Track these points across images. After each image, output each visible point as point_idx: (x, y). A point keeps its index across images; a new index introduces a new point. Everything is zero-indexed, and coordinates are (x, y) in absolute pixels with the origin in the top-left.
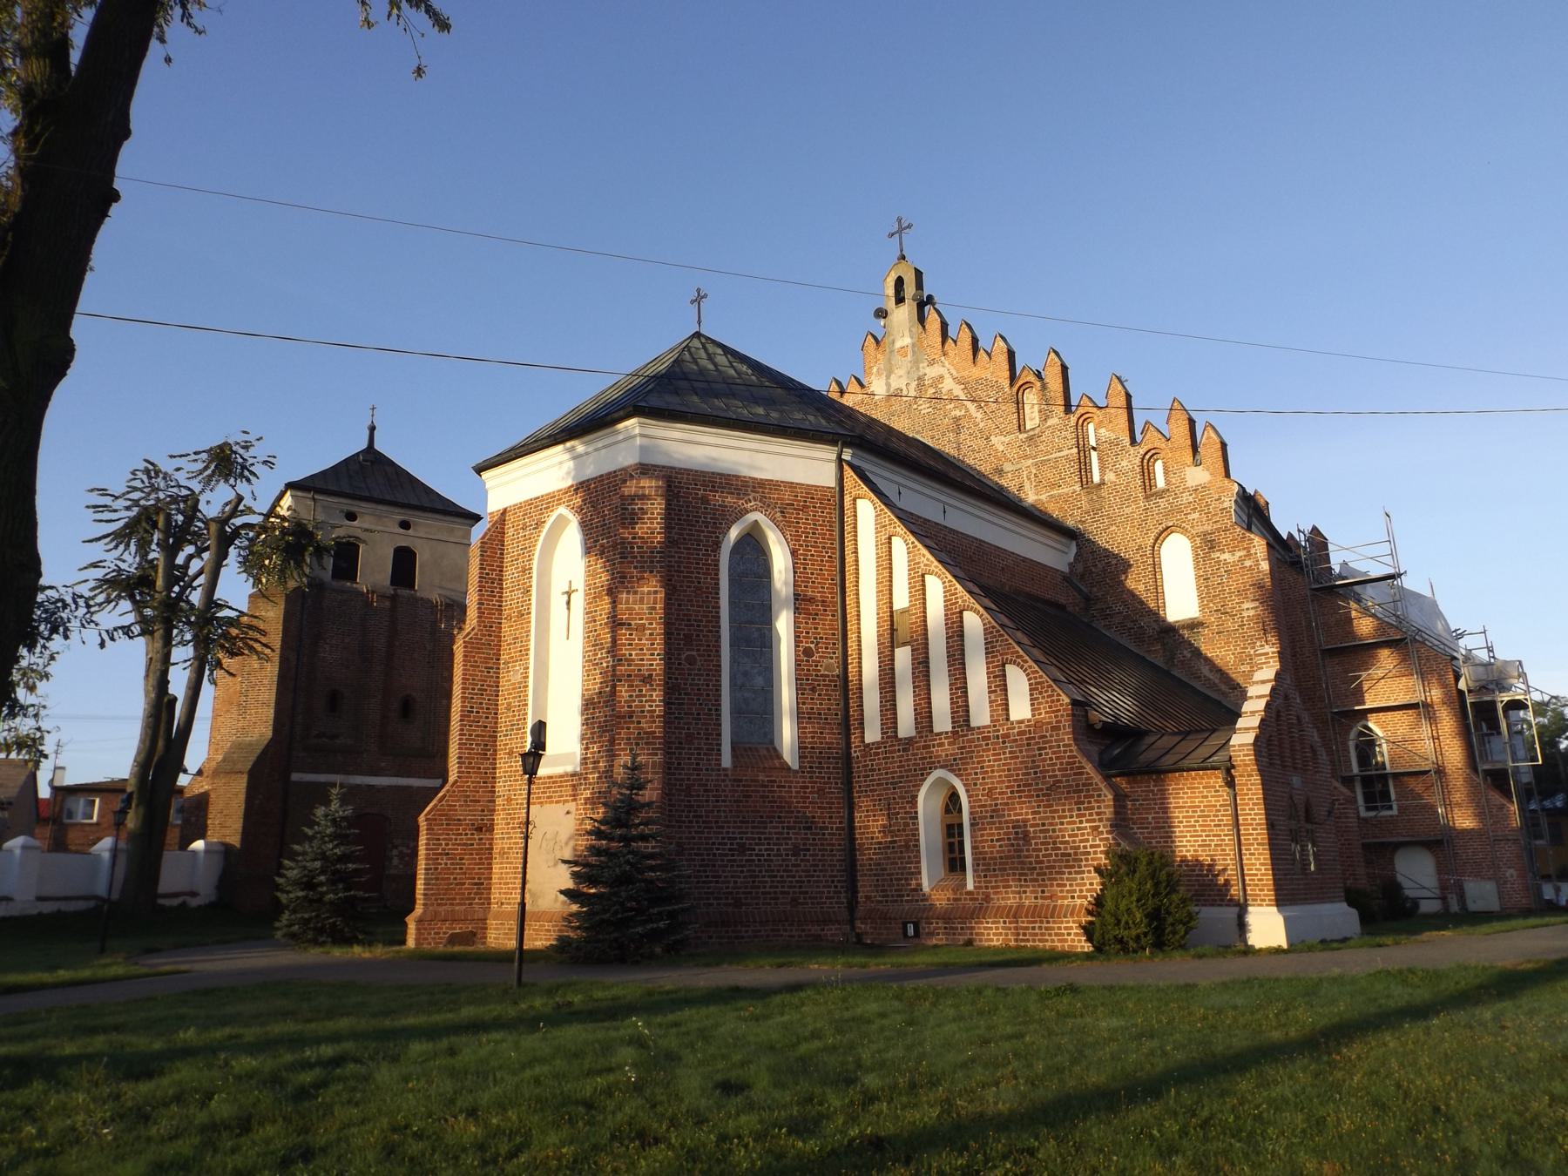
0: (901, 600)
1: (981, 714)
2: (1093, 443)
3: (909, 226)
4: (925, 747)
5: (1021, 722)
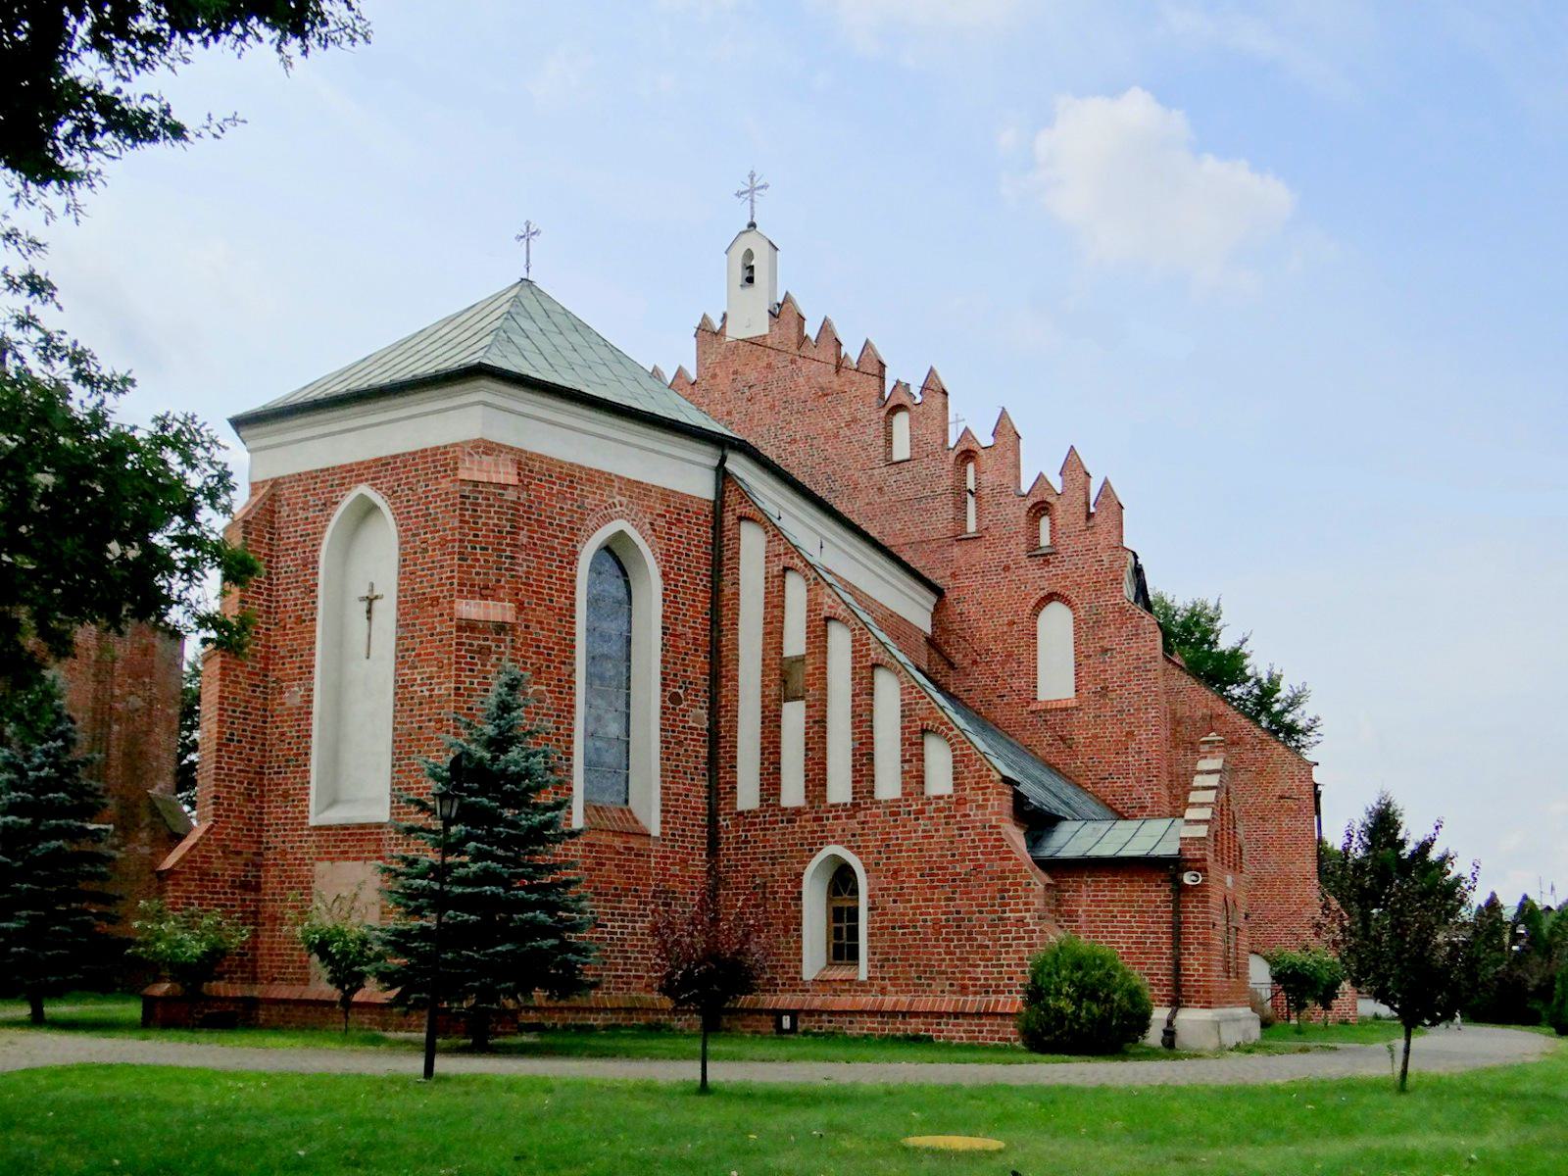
0: (795, 643)
1: (888, 785)
2: (971, 485)
3: (739, 194)
4: (815, 819)
5: (940, 797)
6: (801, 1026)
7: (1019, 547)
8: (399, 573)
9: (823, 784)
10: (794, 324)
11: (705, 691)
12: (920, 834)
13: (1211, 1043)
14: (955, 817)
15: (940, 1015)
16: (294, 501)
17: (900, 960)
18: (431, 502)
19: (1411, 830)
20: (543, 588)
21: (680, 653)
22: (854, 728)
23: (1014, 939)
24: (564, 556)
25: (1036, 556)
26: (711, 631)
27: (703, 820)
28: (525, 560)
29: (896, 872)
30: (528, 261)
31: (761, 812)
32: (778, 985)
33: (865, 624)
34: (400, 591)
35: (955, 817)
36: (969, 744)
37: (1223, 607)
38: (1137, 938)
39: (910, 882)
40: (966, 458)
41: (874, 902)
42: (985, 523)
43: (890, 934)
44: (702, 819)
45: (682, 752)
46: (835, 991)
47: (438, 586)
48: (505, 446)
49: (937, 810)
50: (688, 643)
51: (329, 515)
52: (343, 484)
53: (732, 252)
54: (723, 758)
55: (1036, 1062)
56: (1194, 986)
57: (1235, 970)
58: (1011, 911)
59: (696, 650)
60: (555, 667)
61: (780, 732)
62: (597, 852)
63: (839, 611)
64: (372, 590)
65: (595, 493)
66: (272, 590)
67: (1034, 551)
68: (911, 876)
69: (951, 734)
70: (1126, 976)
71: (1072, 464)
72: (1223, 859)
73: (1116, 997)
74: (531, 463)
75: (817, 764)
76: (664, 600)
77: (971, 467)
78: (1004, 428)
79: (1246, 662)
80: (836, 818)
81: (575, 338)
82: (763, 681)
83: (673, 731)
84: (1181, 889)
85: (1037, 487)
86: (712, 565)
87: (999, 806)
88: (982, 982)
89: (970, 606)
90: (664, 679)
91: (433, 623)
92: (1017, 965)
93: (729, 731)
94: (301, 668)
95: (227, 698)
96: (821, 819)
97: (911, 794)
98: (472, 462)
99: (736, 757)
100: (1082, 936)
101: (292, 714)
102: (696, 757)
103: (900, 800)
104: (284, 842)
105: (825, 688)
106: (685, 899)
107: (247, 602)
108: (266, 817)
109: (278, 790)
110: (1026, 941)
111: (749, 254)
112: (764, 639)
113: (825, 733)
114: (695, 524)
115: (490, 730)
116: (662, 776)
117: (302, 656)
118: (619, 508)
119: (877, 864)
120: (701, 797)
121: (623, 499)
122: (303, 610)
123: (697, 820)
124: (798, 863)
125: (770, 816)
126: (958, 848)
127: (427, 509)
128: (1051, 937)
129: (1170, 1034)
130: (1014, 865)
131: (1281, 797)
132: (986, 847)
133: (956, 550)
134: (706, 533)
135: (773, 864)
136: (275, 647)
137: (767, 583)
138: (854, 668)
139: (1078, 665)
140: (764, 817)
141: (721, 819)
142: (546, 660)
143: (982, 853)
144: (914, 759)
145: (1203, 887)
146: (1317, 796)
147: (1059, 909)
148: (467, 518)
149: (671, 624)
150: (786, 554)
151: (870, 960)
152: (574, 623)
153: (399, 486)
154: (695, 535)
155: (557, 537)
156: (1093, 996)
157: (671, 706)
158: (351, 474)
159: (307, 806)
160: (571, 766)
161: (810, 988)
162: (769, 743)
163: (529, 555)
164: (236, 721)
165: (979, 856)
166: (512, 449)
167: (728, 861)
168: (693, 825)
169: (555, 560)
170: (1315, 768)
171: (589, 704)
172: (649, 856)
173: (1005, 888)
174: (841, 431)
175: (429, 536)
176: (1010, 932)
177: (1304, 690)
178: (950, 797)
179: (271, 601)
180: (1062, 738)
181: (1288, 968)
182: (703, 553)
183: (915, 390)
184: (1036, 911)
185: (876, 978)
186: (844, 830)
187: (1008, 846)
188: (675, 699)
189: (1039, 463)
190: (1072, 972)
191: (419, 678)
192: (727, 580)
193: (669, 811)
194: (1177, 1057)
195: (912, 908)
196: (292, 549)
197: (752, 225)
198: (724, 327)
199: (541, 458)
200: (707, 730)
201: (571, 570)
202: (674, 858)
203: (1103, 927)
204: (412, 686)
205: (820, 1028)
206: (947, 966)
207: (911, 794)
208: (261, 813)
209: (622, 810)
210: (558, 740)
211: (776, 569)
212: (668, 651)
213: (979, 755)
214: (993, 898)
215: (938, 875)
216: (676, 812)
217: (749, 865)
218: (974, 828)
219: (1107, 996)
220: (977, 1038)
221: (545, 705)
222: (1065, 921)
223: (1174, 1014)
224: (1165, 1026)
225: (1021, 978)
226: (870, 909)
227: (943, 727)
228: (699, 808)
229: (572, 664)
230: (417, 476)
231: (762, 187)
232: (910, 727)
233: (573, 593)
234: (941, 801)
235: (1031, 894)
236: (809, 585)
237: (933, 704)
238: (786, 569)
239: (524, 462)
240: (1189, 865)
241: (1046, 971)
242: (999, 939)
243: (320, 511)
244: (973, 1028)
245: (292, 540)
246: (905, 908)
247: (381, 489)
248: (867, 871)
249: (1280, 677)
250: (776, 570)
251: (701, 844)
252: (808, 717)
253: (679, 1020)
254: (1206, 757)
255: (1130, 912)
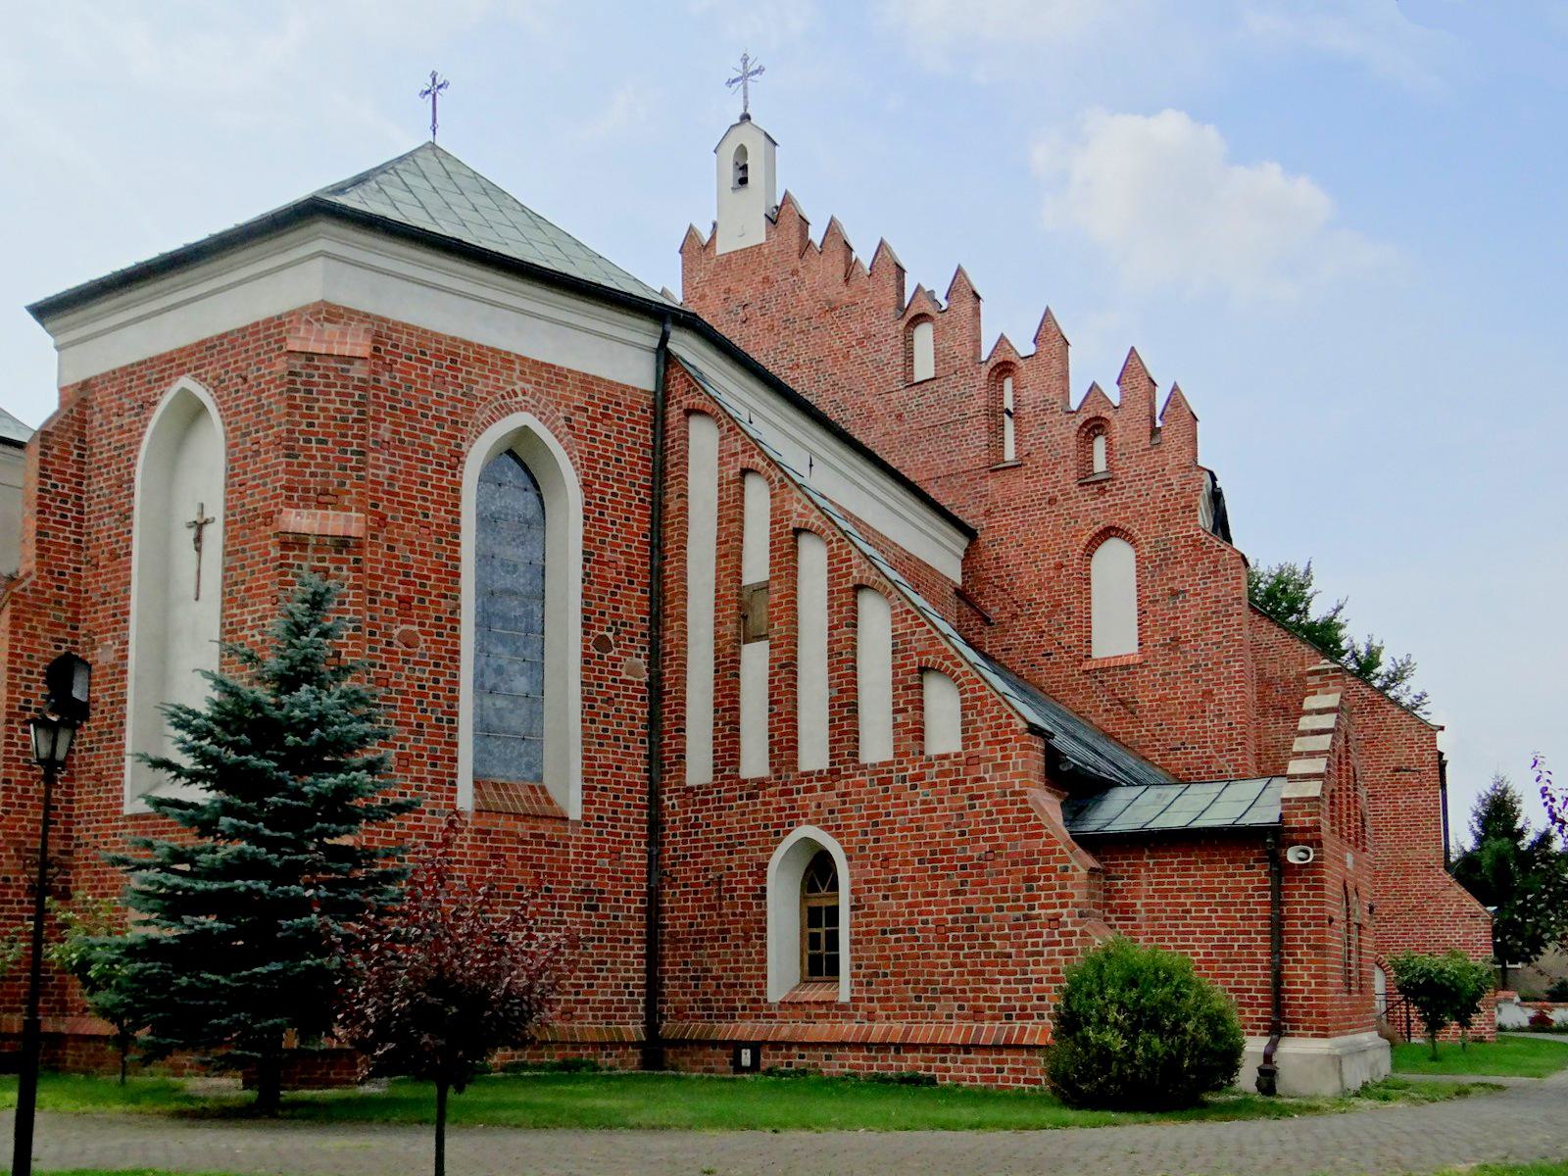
0: (756, 567)
1: (877, 744)
2: (1009, 404)
4: (783, 793)
5: (946, 757)
6: (766, 1062)
7: (1066, 477)
8: (226, 486)
9: (793, 746)
10: (795, 227)
11: (643, 635)
12: (918, 806)
13: (1329, 1087)
14: (964, 781)
15: (945, 1048)
16: (107, 405)
17: (893, 974)
18: (263, 391)
19: (1531, 818)
20: (415, 498)
21: (609, 585)
22: (831, 671)
23: (1045, 945)
24: (443, 458)
25: (1088, 484)
26: (651, 558)
27: (641, 799)
28: (390, 462)
29: (886, 859)
30: (434, 121)
31: (714, 786)
32: (736, 1009)
33: (844, 533)
34: (228, 508)
35: (964, 781)
36: (983, 683)
37: (1314, 572)
38: (1219, 940)
39: (904, 871)
40: (1000, 373)
41: (858, 900)
42: (1026, 447)
43: (879, 941)
44: (640, 798)
45: (612, 712)
46: (809, 1016)
47: (273, 497)
48: (357, 312)
49: (941, 774)
50: (619, 573)
51: (146, 419)
52: (162, 379)
53: (720, 151)
54: (668, 719)
55: (1066, 1125)
56: (1301, 1006)
57: (1355, 983)
58: (1043, 906)
59: (631, 582)
60: (431, 602)
61: (738, 683)
62: (493, 840)
63: (812, 520)
64: (202, 514)
65: (487, 377)
66: (83, 520)
67: (1086, 479)
68: (906, 863)
69: (958, 671)
70: (1203, 995)
71: (1133, 370)
72: (1341, 829)
73: (1189, 1026)
74: (394, 335)
75: (784, 721)
76: (586, 518)
77: (1008, 383)
78: (1048, 332)
79: (1341, 633)
80: (809, 790)
81: (481, 201)
82: (716, 618)
83: (600, 686)
84: (1282, 871)
85: (1089, 401)
86: (652, 475)
87: (1025, 766)
88: (1002, 1003)
89: (1006, 545)
90: (587, 619)
91: (266, 546)
92: (1050, 980)
93: (675, 685)
94: (114, 615)
95: (20, 656)
96: (790, 792)
97: (906, 754)
98: (308, 331)
99: (684, 718)
100: (1141, 938)
101: (107, 674)
102: (633, 719)
103: (891, 763)
104: (96, 836)
105: (794, 622)
106: (617, 900)
107: (47, 535)
108: (76, 805)
109: (89, 771)
110: (1063, 947)
111: (742, 151)
112: (718, 564)
113: (795, 680)
114: (628, 420)
115: (273, 663)
116: (583, 743)
117: (116, 600)
118: (521, 398)
119: (862, 849)
120: (639, 770)
121: (527, 386)
122: (117, 542)
123: (634, 799)
124: (761, 850)
125: (726, 791)
126: (970, 824)
127: (259, 400)
128: (1097, 941)
129: (1268, 1078)
130: (1045, 844)
131: (1397, 770)
132: (1006, 820)
133: (990, 482)
134: (644, 434)
135: (730, 853)
136: (87, 592)
137: (720, 491)
138: (831, 593)
139: (1142, 612)
140: (719, 792)
141: (665, 797)
142: (419, 592)
143: (1001, 829)
144: (910, 708)
145: (1315, 868)
146: (1442, 766)
147: (1111, 905)
148: (298, 402)
149: (596, 548)
150: (744, 452)
151: (853, 975)
152: (459, 545)
153: (227, 372)
154: (629, 435)
155: (434, 433)
156: (1154, 1025)
157: (597, 653)
158: (168, 365)
159: (122, 789)
160: (456, 729)
161: (777, 1012)
162: (723, 697)
163: (393, 455)
164: (33, 685)
165: (998, 834)
166: (367, 316)
167: (675, 850)
168: (628, 806)
169: (431, 463)
170: (1439, 734)
171: (481, 650)
172: (566, 846)
173: (1033, 873)
174: (852, 351)
175: (261, 434)
176: (1040, 935)
177: (1408, 663)
178: (957, 755)
179: (82, 535)
180: (1122, 702)
181: (1420, 977)
182: (639, 458)
183: (940, 297)
184: (1076, 905)
185: (862, 999)
186: (819, 806)
187: (1036, 819)
188: (602, 644)
189: (1092, 369)
190: (1123, 990)
191: (250, 618)
192: (672, 493)
193: (594, 788)
194: (1282, 1112)
195: (909, 905)
196: (106, 466)
197: (746, 117)
198: (713, 237)
199: (410, 330)
200: (647, 684)
201: (454, 475)
202: (602, 848)
203: (1171, 926)
204: (242, 629)
205: (789, 1064)
206: (955, 983)
207: (906, 754)
208: (70, 802)
209: (532, 788)
210: (436, 696)
211: (732, 472)
212: (591, 583)
213: (997, 698)
214: (1016, 890)
215: (942, 861)
216: (604, 789)
217: (701, 855)
218: (990, 796)
219: (1176, 1024)
220: (995, 1079)
221: (418, 650)
222: (1117, 919)
223: (1273, 1045)
224: (1261, 1062)
225: (1053, 1001)
226: (853, 908)
227: (947, 663)
228: (636, 784)
229: (456, 598)
230: (247, 358)
231: (757, 72)
232: (905, 665)
233: (456, 506)
234: (946, 762)
235: (1069, 883)
236: (772, 489)
237: (935, 634)
238: (745, 472)
239: (385, 338)
240: (1294, 836)
241: (1084, 989)
242: (1025, 945)
243: (137, 415)
244: (991, 1066)
245: (105, 455)
246: (899, 906)
247: (205, 380)
248: (849, 859)
249: (1379, 649)
250: (732, 473)
251: (639, 829)
252: (772, 660)
253: (609, 1055)
254: (1315, 693)
255: (1210, 904)
